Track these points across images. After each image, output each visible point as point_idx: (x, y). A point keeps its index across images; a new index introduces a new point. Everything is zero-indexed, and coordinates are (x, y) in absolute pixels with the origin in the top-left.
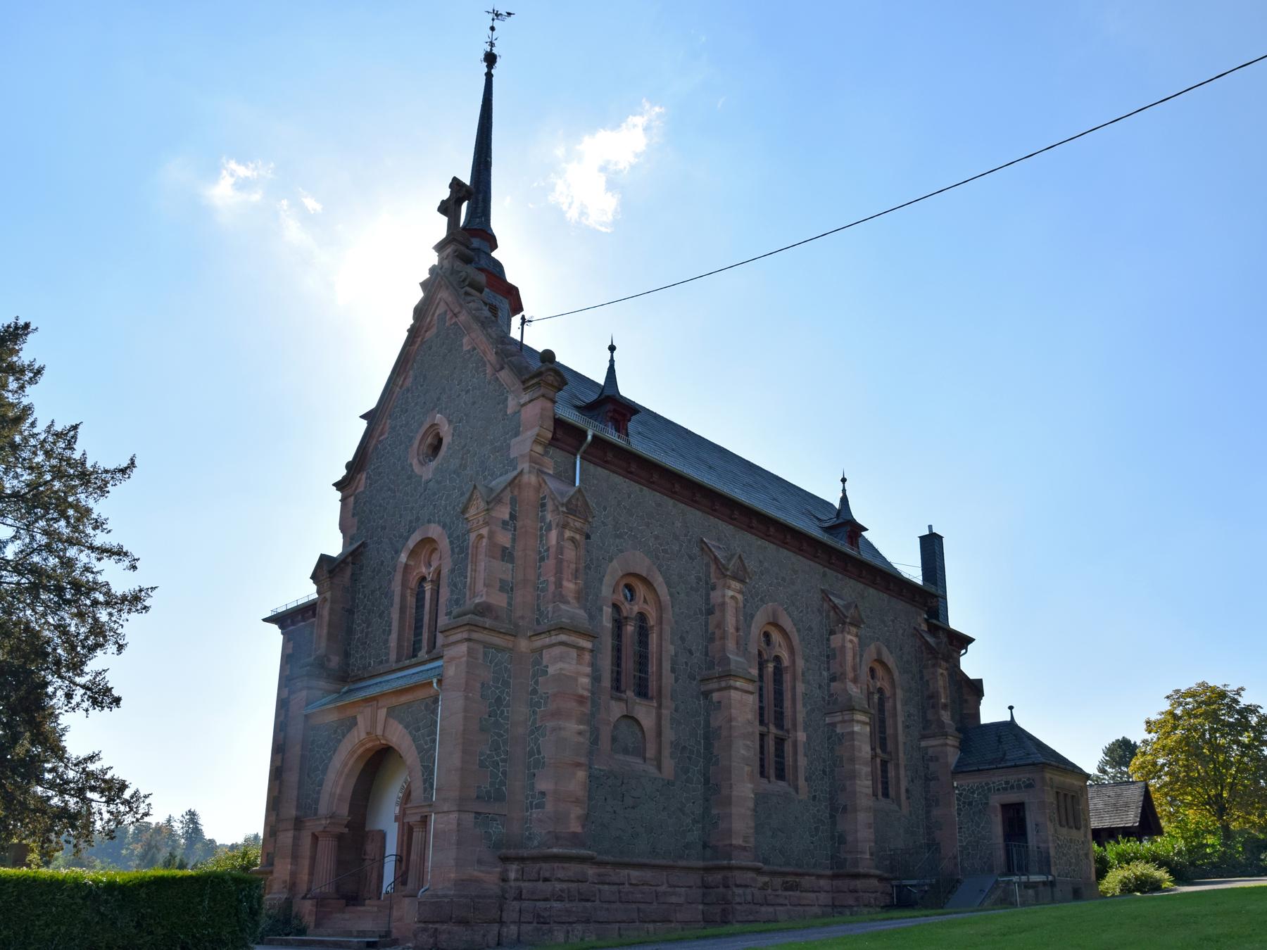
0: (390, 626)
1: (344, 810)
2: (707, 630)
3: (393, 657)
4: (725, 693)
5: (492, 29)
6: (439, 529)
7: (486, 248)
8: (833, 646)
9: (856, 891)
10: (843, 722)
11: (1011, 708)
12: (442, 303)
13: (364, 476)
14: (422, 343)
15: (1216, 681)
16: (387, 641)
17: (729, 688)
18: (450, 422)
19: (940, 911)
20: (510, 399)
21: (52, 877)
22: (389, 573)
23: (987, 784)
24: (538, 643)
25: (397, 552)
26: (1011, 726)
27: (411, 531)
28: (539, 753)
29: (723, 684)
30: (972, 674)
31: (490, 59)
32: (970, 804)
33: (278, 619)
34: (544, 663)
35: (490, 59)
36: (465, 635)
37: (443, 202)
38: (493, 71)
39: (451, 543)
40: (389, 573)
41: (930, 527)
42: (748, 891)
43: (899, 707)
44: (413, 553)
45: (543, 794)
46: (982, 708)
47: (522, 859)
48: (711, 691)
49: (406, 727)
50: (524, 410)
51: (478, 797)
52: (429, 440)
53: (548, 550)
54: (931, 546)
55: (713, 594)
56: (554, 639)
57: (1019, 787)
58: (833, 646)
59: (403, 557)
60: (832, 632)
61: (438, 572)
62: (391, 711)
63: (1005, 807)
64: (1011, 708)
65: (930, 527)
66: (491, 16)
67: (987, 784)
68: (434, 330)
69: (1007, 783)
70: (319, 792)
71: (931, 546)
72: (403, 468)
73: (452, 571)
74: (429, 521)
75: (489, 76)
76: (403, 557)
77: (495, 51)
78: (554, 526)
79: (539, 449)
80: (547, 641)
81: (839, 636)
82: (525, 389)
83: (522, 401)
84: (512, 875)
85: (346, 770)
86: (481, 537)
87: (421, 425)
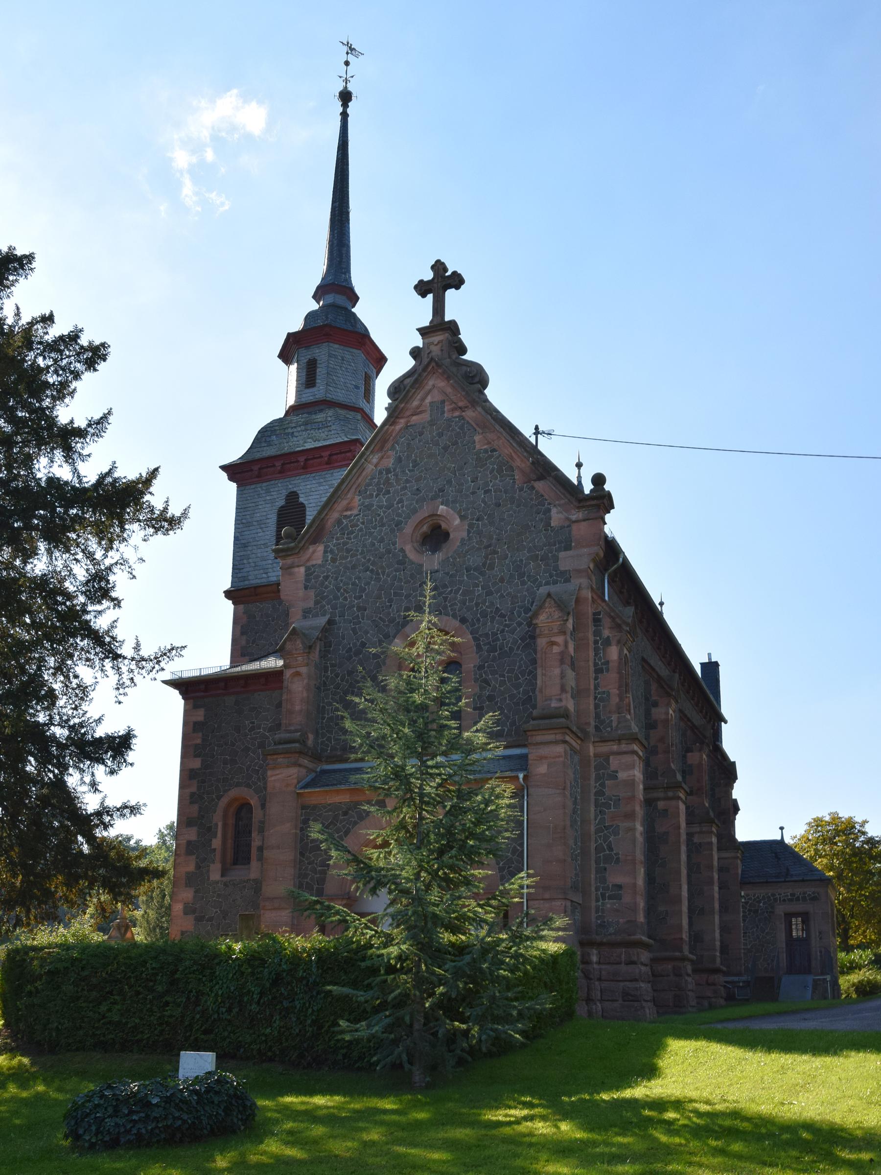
4: (673, 803)
5: (347, 63)
7: (348, 304)
8: (689, 762)
9: (714, 984)
10: (701, 832)
11: (782, 828)
12: (435, 392)
15: (844, 814)
18: (463, 518)
19: (770, 1007)
20: (554, 511)
21: (65, 947)
23: (773, 895)
24: (604, 748)
28: (610, 849)
29: (670, 794)
31: (346, 97)
32: (756, 911)
34: (612, 768)
35: (346, 97)
36: (559, 737)
37: (421, 282)
38: (349, 111)
39: (475, 639)
41: (709, 655)
45: (620, 887)
47: (601, 944)
48: (658, 799)
50: (574, 527)
52: (425, 528)
55: (654, 710)
56: (624, 747)
57: (804, 899)
58: (689, 762)
60: (689, 750)
64: (782, 828)
65: (709, 655)
66: (345, 49)
67: (773, 895)
69: (793, 895)
75: (344, 116)
77: (350, 88)
78: (614, 642)
80: (615, 748)
82: (578, 508)
84: (594, 959)
87: (415, 511)
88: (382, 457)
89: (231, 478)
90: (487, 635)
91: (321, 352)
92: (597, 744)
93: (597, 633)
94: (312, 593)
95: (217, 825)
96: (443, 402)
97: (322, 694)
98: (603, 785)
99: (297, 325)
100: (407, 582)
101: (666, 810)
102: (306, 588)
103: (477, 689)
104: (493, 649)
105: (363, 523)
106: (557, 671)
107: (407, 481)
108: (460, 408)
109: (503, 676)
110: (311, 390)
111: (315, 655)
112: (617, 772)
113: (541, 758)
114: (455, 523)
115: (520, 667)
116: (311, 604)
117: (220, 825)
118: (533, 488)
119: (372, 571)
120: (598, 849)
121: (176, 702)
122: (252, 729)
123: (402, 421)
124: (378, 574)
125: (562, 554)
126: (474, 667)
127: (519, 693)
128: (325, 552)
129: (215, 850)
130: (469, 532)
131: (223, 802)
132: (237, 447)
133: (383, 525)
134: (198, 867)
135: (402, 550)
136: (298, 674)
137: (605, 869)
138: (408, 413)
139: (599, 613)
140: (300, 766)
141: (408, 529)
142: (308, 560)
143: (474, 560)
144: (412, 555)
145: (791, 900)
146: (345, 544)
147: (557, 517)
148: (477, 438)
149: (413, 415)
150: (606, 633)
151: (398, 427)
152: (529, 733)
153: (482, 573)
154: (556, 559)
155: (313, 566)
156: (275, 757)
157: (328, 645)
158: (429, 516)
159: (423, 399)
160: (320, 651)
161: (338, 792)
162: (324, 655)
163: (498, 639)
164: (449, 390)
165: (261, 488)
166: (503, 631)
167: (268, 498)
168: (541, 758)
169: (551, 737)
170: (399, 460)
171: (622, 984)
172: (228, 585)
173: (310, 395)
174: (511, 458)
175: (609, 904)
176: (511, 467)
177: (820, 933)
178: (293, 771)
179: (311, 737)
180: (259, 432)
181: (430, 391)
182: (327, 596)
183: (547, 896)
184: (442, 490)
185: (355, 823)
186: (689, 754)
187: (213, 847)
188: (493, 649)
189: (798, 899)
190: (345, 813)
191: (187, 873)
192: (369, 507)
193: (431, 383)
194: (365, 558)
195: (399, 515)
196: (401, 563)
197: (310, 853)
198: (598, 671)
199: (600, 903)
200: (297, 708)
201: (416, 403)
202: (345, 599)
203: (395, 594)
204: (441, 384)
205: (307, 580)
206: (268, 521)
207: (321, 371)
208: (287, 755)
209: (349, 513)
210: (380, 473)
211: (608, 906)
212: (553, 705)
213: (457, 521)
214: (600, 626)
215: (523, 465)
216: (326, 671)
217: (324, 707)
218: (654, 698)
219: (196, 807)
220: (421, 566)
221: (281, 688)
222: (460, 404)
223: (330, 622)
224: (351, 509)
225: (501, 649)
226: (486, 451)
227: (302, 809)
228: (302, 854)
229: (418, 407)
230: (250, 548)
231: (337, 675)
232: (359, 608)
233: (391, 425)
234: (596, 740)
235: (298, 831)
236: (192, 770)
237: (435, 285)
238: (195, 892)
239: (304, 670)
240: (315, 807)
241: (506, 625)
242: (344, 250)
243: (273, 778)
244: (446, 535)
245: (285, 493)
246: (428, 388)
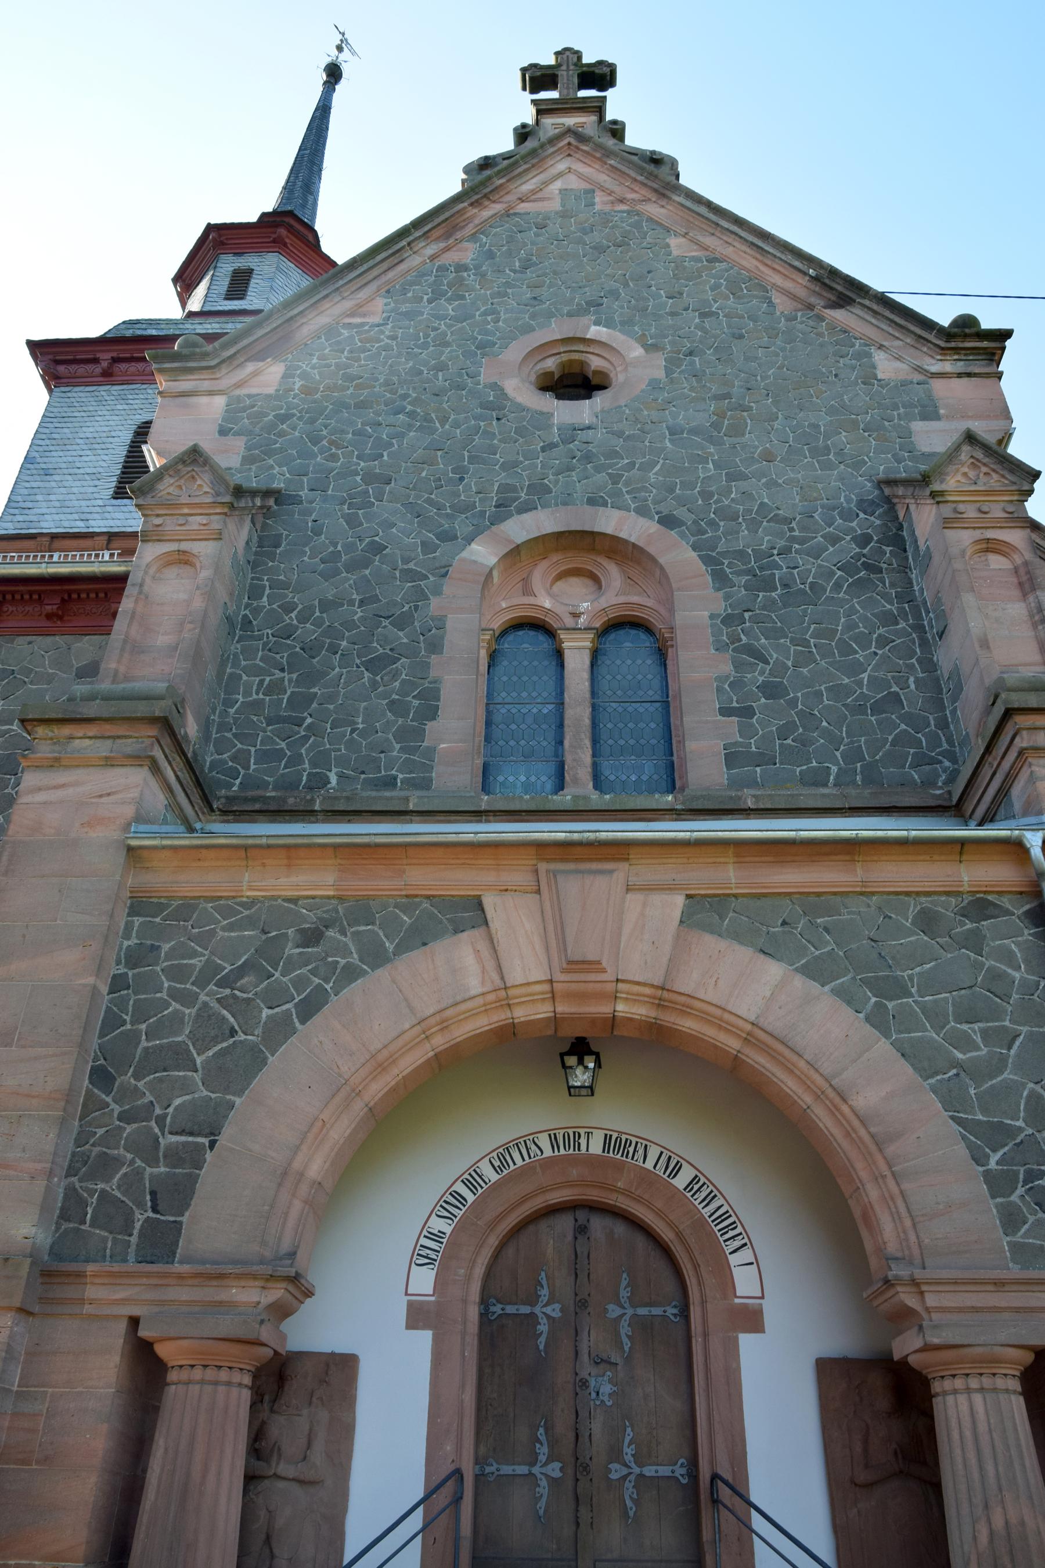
6: (652, 527)
14: (508, 214)
35: (334, 73)
37: (534, 66)
44: (514, 555)
59: (483, 553)
62: (705, 911)
76: (483, 553)
90: (741, 554)
103: (727, 668)
114: (633, 362)
115: (850, 627)
119: (412, 415)
124: (427, 419)
126: (712, 617)
127: (860, 684)
141: (515, 352)
142: (239, 385)
151: (486, 214)
155: (249, 396)
156: (66, 730)
161: (291, 852)
166: (784, 552)
180: (124, 323)
182: (281, 450)
185: (351, 974)
190: (312, 937)
195: (487, 333)
197: (137, 1076)
208: (108, 729)
209: (357, 320)
217: (235, 678)
227: (133, 911)
228: (102, 1077)
230: (57, 478)
231: (288, 608)
232: (369, 478)
233: (471, 204)
235: (104, 989)
240: (186, 909)
241: (793, 539)
242: (310, 198)
243: (41, 797)
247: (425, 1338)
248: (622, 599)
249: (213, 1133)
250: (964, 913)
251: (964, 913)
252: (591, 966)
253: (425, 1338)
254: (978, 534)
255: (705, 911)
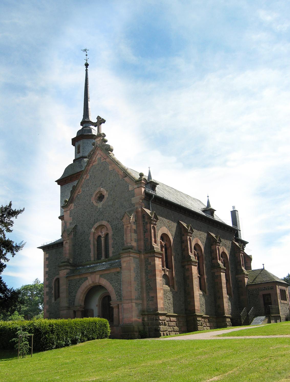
0: (90, 250)
1: (83, 304)
2: (182, 248)
3: (92, 259)
5: (87, 55)
6: (106, 222)
11: (263, 265)
12: (99, 155)
13: (73, 204)
14: (92, 166)
16: (89, 255)
17: (155, 256)
18: (107, 191)
20: (130, 186)
22: (88, 235)
25: (90, 228)
26: (263, 270)
27: (95, 222)
28: (150, 286)
30: (248, 254)
31: (87, 65)
32: (253, 294)
33: (45, 248)
35: (87, 65)
38: (88, 69)
39: (112, 227)
40: (88, 235)
42: (200, 322)
43: (229, 266)
44: (96, 229)
46: (252, 264)
49: (107, 280)
51: (136, 299)
52: (98, 195)
53: (147, 230)
54: (234, 214)
59: (93, 230)
61: (107, 235)
62: (101, 276)
63: (264, 296)
64: (263, 265)
68: (97, 163)
70: (74, 299)
71: (234, 214)
72: (89, 203)
73: (113, 235)
74: (102, 220)
75: (86, 70)
76: (93, 230)
78: (148, 223)
79: (141, 201)
81: (214, 246)
82: (136, 184)
83: (135, 187)
85: (84, 292)
86: (128, 227)
87: (95, 191)
88: (87, 176)
89: (58, 184)
91: (80, 142)
92: (145, 255)
93: (144, 221)
94: (71, 218)
95: (53, 287)
96: (101, 157)
97: (75, 247)
98: (147, 267)
99: (75, 136)
100: (94, 212)
101: (188, 269)
102: (70, 216)
104: (116, 229)
105: (83, 196)
106: (130, 235)
107: (93, 182)
108: (105, 159)
109: (119, 237)
110: (79, 154)
111: (72, 236)
112: (150, 262)
113: (124, 261)
114: (105, 193)
116: (71, 221)
117: (54, 286)
118: (124, 180)
120: (147, 286)
121: (41, 252)
122: (60, 258)
123: (91, 165)
125: (132, 199)
126: (112, 235)
128: (74, 205)
129: (53, 294)
130: (109, 195)
131: (54, 279)
132: (59, 174)
133: (88, 196)
134: (49, 299)
135: (93, 203)
136: (67, 242)
137: (149, 292)
138: (92, 162)
139: (144, 215)
140: (67, 269)
141: (94, 196)
142: (70, 209)
143: (110, 203)
144: (95, 204)
145: (264, 290)
146: (79, 202)
147: (130, 188)
148: (110, 167)
149: (93, 163)
150: (146, 220)
152: (121, 254)
153: (112, 207)
154: (131, 200)
157: (76, 232)
158: (99, 192)
159: (96, 158)
160: (74, 234)
162: (75, 235)
163: (117, 226)
164: (102, 154)
165: (66, 186)
167: (68, 188)
168: (124, 261)
169: (126, 255)
170: (91, 176)
171: (154, 326)
172: (59, 215)
173: (78, 156)
174: (118, 171)
175: (150, 303)
176: (119, 174)
177: (275, 300)
178: (65, 271)
179: (71, 260)
181: (97, 155)
183: (127, 302)
184: (101, 184)
186: (212, 246)
187: (52, 293)
188: (116, 229)
189: (266, 289)
190: (79, 282)
191: (47, 301)
192: (84, 191)
193: (98, 152)
194: (83, 206)
196: (92, 206)
198: (145, 232)
199: (148, 303)
200: (67, 252)
201: (94, 159)
202: (79, 219)
203: (92, 216)
204: (100, 152)
205: (70, 214)
206: (68, 195)
207: (81, 148)
210: (86, 181)
211: (150, 303)
212: (129, 245)
213: (106, 192)
214: (144, 218)
215: (121, 173)
216: (76, 240)
218: (183, 233)
219: (48, 282)
220: (97, 206)
221: (63, 247)
222: (105, 158)
223: (76, 226)
224: (80, 192)
225: (118, 229)
226: (112, 170)
229: (95, 160)
234: (145, 253)
236: (46, 272)
237: (98, 123)
238: (49, 306)
239: (68, 241)
244: (104, 196)
245: (72, 186)
246: (97, 154)
247: (97, 307)
248: (106, 232)
249: (75, 297)
250: (117, 273)
251: (117, 273)
252: (94, 282)
253: (97, 307)
254: (126, 226)
255: (101, 276)
